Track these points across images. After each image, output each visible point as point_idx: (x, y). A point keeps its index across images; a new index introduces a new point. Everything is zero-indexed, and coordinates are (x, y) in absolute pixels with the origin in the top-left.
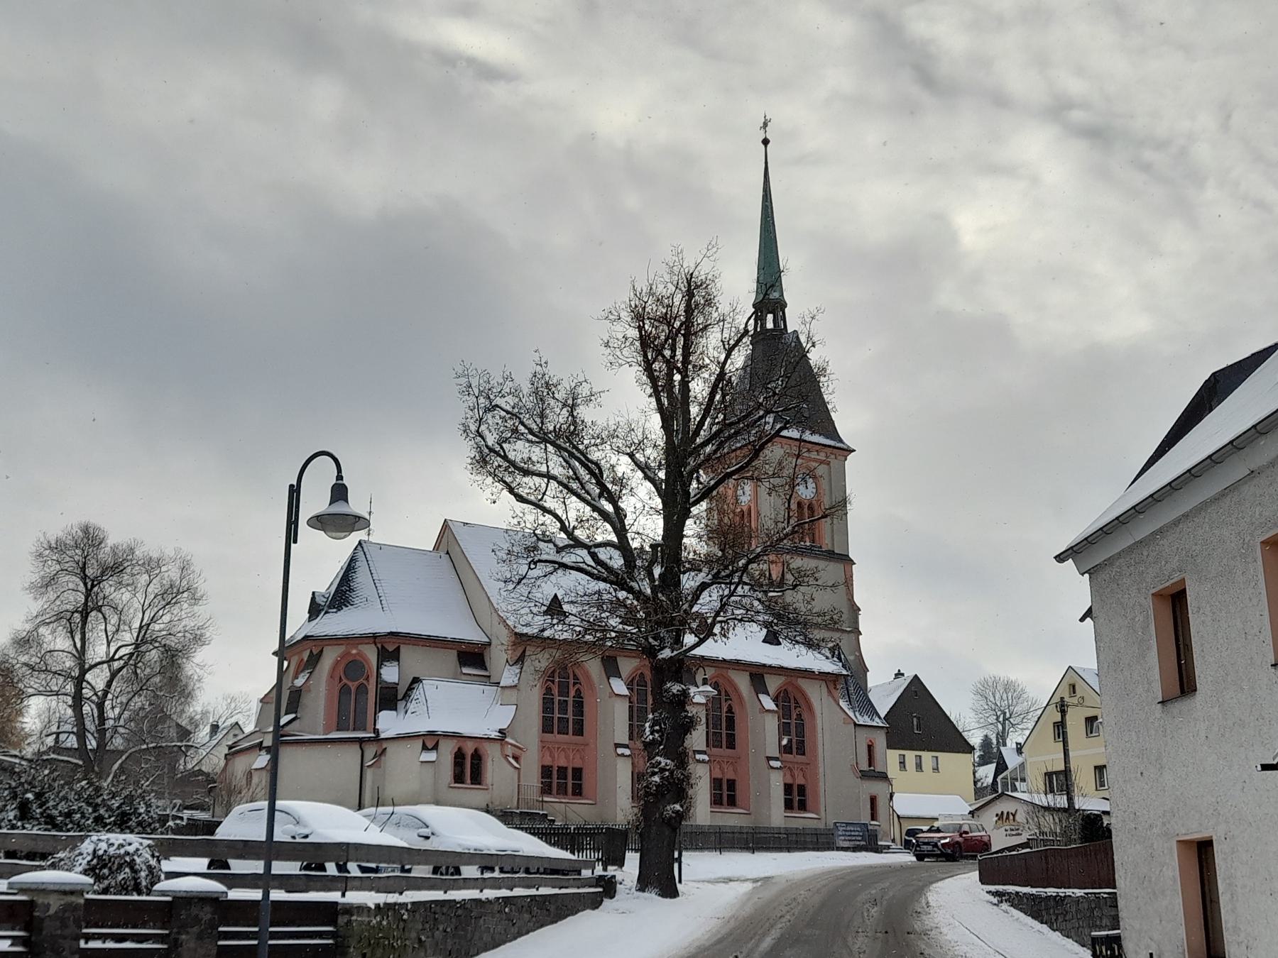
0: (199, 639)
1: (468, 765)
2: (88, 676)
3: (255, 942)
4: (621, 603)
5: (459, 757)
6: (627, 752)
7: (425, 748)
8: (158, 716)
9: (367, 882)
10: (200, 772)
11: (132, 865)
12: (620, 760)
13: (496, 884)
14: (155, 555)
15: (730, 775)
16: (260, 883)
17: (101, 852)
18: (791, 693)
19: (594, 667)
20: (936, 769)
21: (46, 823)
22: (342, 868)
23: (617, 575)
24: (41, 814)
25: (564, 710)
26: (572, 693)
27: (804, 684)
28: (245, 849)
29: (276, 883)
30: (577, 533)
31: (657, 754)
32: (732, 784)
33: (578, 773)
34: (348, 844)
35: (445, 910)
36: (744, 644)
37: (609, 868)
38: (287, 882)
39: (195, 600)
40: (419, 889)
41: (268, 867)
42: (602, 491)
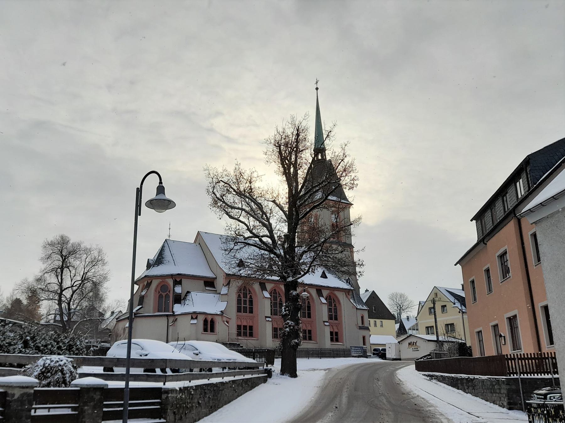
0: (105, 278)
1: (209, 325)
2: (64, 293)
3: (122, 409)
4: (271, 259)
5: (205, 321)
6: (270, 319)
7: (192, 318)
8: (92, 308)
9: (176, 377)
10: (107, 329)
11: (62, 371)
12: (268, 323)
13: (228, 375)
14: (89, 247)
16: (125, 378)
17: (47, 365)
18: (331, 295)
19: (257, 287)
20: (382, 326)
21: (36, 349)
22: (163, 370)
23: (269, 247)
24: (34, 345)
25: (245, 304)
26: (248, 297)
27: (337, 293)
28: (118, 362)
29: (132, 378)
30: (254, 231)
31: (288, 320)
32: (337, 334)
33: (251, 328)
34: (166, 359)
35: (209, 388)
36: (313, 278)
37: (269, 366)
38: (137, 378)
39: (104, 264)
40: (198, 379)
41: (128, 371)
42: (263, 217)
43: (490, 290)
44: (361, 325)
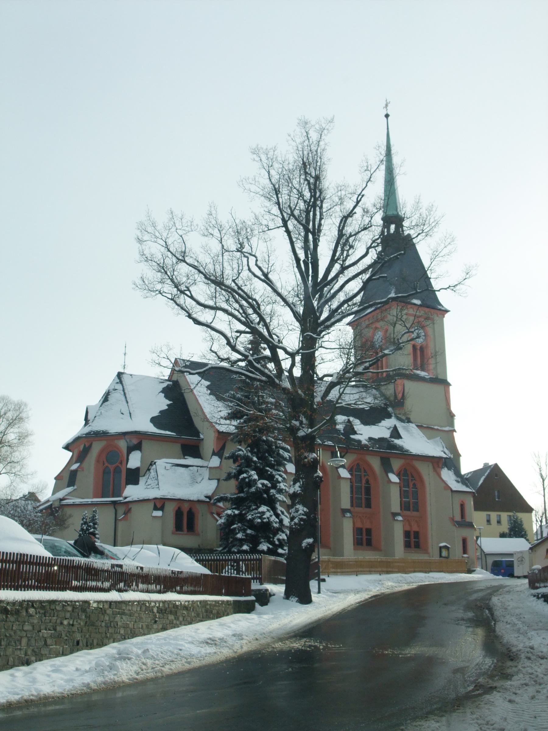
5: (179, 514)
7: (156, 508)
15: (368, 525)
32: (369, 532)
43: (362, 434)
44: (458, 518)
